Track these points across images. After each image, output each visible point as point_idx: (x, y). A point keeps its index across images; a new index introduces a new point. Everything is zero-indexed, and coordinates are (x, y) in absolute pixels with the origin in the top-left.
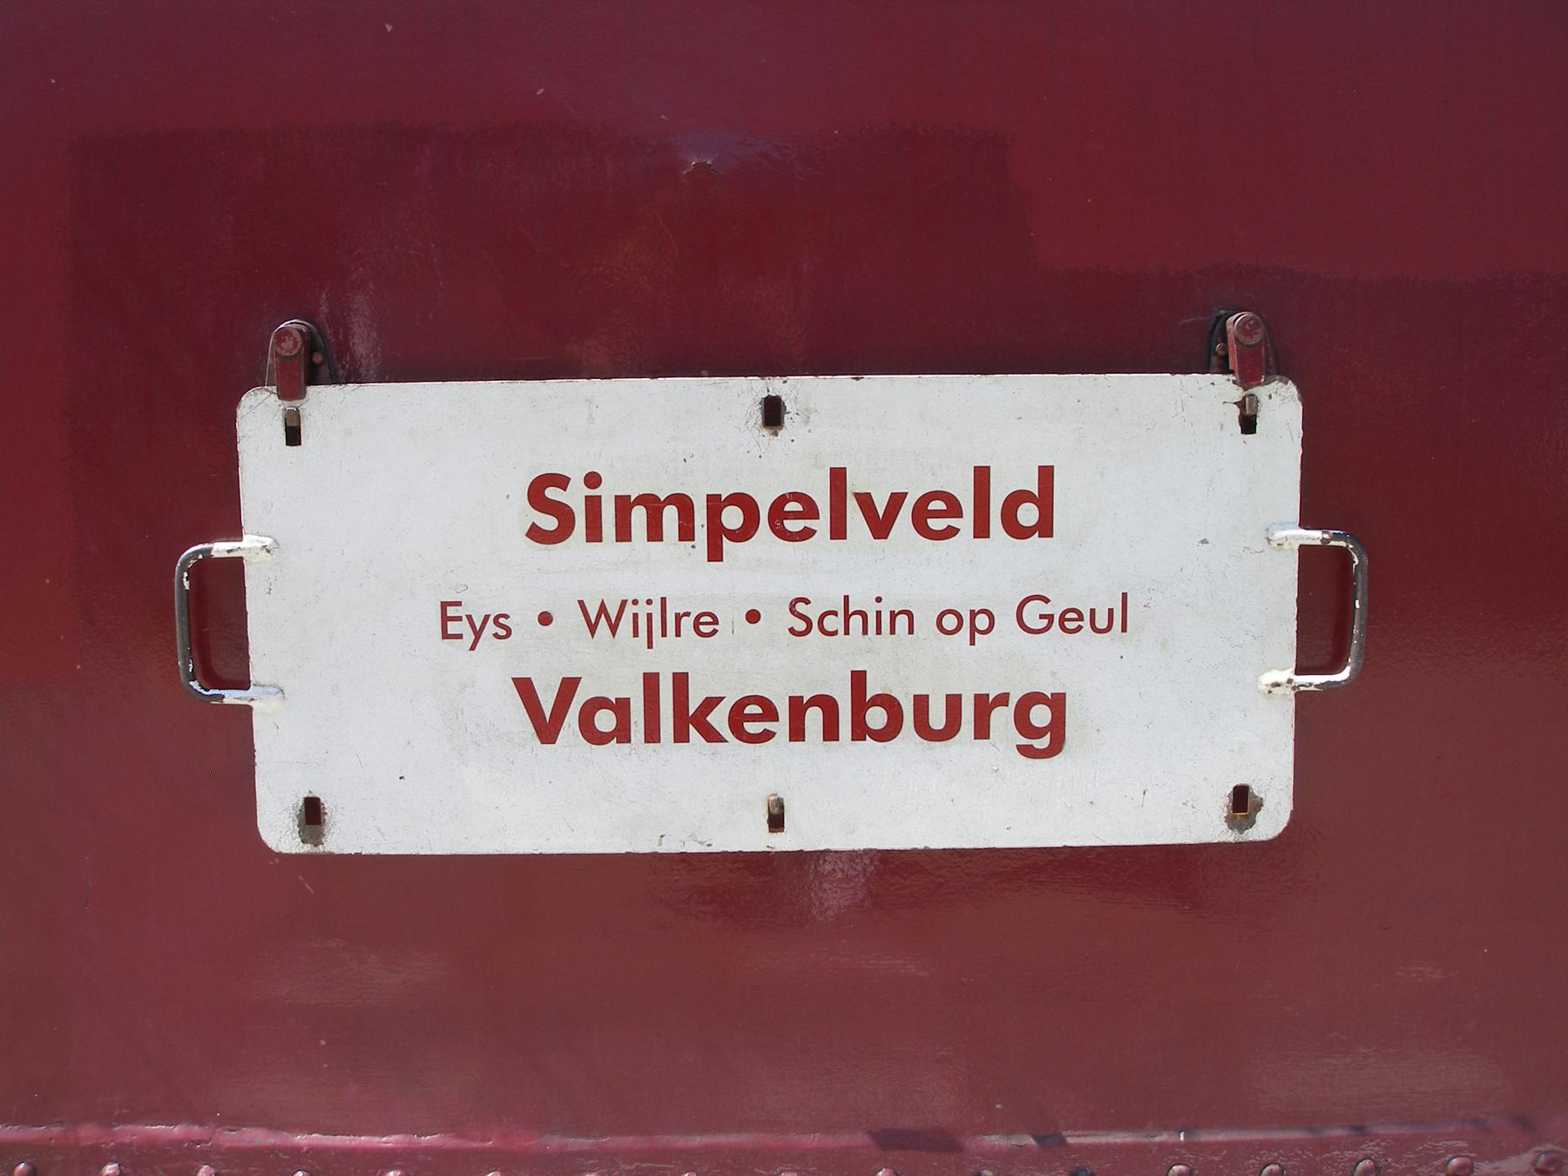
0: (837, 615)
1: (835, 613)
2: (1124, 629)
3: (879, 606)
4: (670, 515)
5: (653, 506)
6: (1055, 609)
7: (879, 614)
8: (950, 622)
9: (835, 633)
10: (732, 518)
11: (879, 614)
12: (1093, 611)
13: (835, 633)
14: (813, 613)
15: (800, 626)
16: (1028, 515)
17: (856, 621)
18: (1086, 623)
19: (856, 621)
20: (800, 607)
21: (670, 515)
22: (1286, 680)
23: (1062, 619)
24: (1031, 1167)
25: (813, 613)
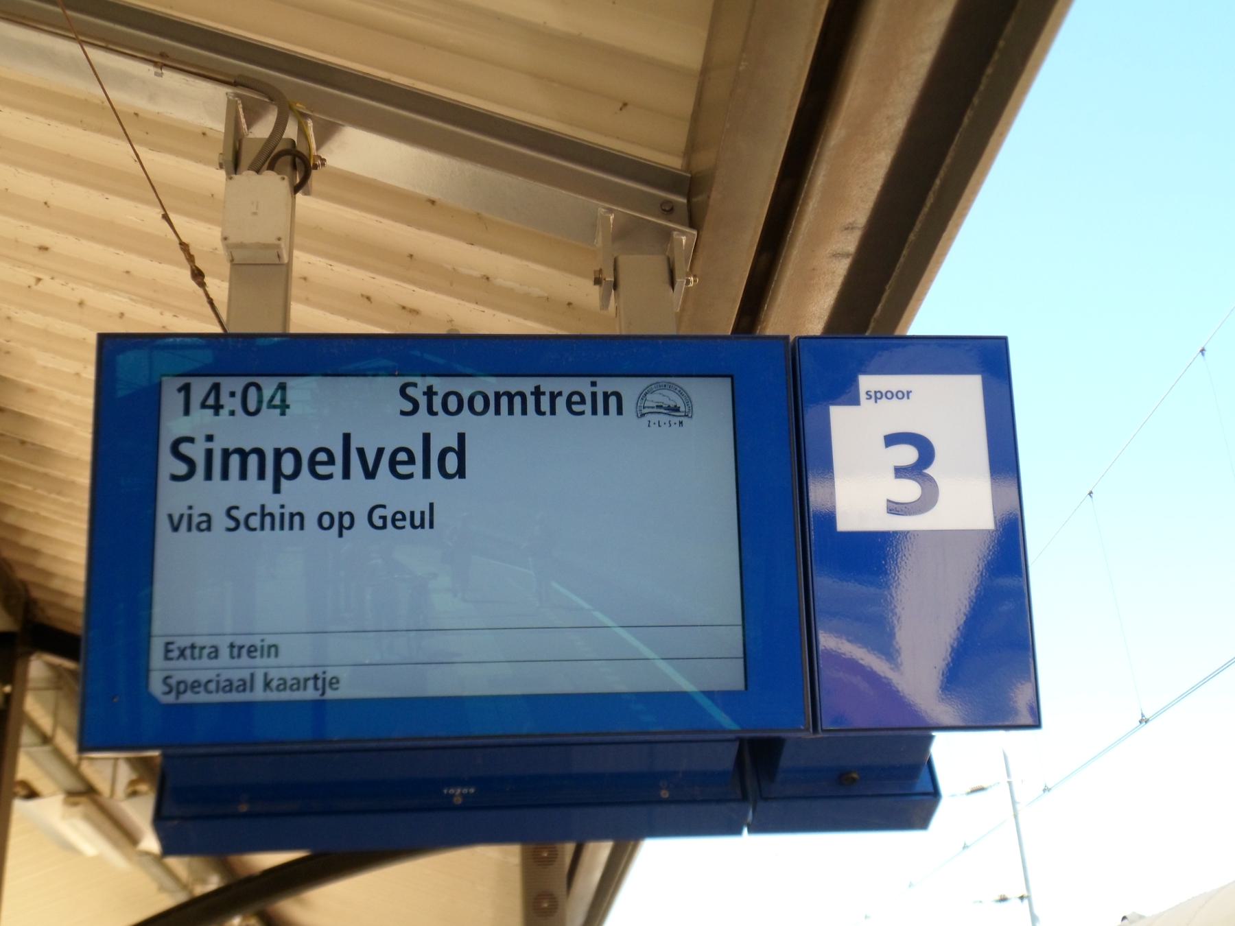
0: (911, 392)
1: (254, 514)
2: (431, 526)
3: (282, 511)
4: (253, 460)
5: (243, 454)
6: (388, 513)
7: (282, 515)
8: (326, 521)
9: (255, 529)
10: (288, 464)
11: (282, 515)
12: (412, 514)
13: (255, 529)
14: (240, 515)
15: (232, 524)
16: (452, 463)
17: (268, 520)
18: (407, 523)
19: (268, 520)
20: (234, 513)
21: (253, 460)
22: (597, 287)
23: (394, 520)
24: (888, 629)
25: (240, 515)
